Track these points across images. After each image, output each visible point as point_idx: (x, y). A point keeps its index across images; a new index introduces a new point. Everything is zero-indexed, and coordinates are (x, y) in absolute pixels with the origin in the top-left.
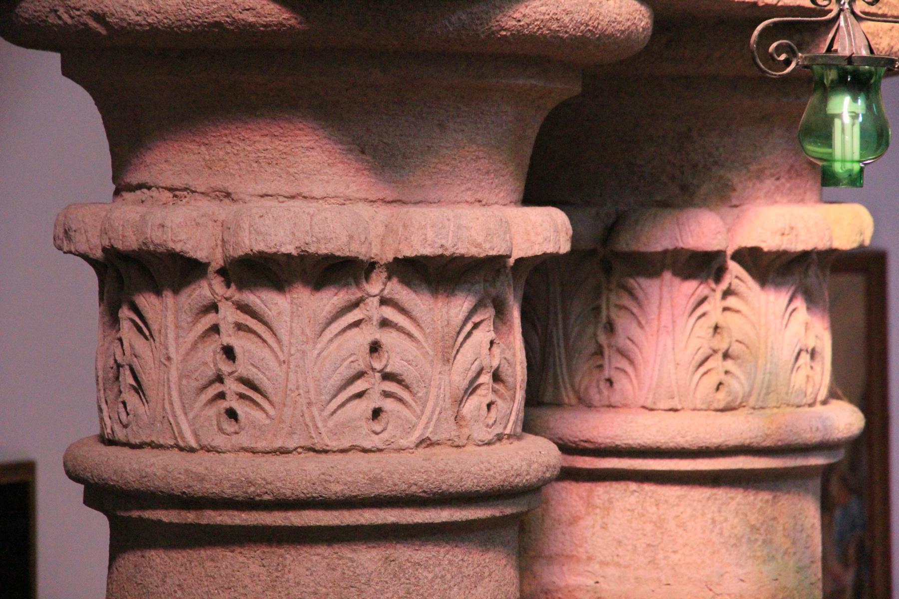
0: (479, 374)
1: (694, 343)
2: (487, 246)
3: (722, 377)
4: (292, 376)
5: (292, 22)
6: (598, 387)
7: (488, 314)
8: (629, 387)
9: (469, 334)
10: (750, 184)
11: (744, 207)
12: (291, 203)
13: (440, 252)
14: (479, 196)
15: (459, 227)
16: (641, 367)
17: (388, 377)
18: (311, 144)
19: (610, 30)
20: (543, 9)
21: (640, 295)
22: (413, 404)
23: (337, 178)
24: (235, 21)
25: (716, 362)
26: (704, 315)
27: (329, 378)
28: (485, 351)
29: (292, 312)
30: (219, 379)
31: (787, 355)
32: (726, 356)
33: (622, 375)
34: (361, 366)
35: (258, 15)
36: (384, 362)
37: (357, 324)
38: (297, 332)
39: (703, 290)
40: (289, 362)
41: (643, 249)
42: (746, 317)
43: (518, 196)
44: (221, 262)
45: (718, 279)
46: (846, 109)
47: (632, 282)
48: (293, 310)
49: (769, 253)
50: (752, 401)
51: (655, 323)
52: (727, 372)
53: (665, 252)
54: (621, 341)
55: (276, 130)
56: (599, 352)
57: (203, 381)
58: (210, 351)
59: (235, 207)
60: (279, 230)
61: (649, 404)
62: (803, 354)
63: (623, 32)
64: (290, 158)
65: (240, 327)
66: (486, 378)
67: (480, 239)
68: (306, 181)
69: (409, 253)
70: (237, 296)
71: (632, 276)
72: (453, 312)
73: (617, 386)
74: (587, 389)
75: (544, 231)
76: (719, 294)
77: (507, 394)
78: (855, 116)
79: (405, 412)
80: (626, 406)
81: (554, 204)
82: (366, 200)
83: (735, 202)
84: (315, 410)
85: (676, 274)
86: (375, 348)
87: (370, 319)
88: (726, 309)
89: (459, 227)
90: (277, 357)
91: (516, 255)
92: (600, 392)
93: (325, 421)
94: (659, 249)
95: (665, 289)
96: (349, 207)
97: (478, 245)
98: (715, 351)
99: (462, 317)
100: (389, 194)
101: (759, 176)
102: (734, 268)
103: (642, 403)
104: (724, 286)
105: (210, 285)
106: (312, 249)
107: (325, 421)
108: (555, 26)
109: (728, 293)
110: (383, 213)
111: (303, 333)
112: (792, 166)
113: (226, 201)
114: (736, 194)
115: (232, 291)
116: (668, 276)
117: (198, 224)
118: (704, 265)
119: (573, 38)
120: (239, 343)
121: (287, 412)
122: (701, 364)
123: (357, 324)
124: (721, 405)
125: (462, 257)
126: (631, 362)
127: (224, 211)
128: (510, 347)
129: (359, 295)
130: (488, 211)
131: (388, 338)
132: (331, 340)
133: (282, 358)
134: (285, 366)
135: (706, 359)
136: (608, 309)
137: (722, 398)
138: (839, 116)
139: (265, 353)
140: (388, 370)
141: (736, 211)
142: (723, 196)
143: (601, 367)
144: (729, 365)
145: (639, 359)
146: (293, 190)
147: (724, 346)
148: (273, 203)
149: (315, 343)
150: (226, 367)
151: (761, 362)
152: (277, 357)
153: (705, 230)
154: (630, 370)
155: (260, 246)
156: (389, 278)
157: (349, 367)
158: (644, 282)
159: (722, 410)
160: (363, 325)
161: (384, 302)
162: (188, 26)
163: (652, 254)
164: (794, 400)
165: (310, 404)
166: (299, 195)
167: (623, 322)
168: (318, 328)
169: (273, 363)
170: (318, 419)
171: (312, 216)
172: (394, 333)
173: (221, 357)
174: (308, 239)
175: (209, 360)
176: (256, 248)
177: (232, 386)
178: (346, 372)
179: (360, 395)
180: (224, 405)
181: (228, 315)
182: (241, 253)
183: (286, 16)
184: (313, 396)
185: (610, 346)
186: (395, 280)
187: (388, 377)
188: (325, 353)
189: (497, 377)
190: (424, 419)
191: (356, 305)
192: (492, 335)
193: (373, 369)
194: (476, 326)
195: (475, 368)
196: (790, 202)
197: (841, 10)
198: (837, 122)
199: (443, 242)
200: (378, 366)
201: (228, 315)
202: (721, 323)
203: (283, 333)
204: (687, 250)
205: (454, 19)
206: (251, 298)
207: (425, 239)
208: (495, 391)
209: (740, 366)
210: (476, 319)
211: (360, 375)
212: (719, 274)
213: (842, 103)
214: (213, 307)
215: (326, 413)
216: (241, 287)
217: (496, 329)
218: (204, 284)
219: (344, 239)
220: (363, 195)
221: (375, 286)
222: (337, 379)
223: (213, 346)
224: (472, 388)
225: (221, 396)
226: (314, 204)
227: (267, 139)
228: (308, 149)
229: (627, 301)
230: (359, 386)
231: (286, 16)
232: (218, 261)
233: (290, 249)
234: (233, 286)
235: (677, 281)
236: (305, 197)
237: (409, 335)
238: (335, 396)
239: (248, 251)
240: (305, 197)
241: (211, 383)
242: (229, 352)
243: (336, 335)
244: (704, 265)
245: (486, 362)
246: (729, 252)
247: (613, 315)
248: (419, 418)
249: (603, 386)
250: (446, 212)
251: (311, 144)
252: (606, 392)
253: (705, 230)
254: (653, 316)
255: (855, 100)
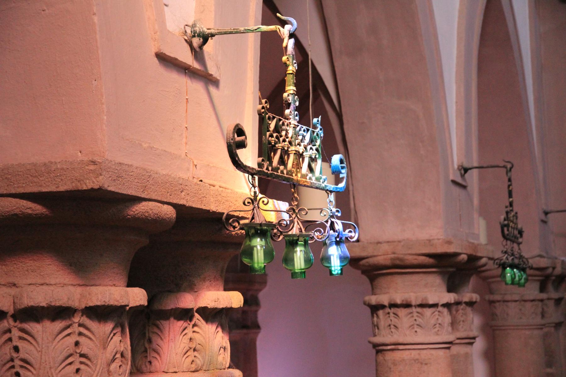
0: (116, 354)
1: (183, 345)
2: (121, 301)
3: (193, 358)
4: (43, 357)
5: (47, 213)
6: (145, 365)
7: (119, 329)
8: (157, 364)
9: (112, 338)
10: (201, 283)
11: (199, 292)
12: (41, 287)
13: (103, 304)
14: (114, 283)
15: (110, 294)
16: (163, 356)
17: (82, 355)
18: (50, 263)
19: (165, 217)
20: (143, 208)
21: (162, 328)
22: (91, 365)
23: (60, 276)
24: (23, 213)
25: (191, 353)
26: (186, 334)
27: (59, 357)
28: (118, 345)
29: (43, 331)
30: (12, 360)
31: (216, 348)
32: (195, 350)
33: (155, 359)
34: (71, 351)
35: (33, 210)
36: (80, 349)
37: (69, 335)
38: (45, 339)
39: (185, 324)
40: (42, 351)
41: (164, 309)
42: (201, 335)
43: (126, 284)
44: (13, 312)
45: (191, 320)
46: (258, 243)
47: (158, 322)
48: (42, 330)
49: (211, 309)
50: (204, 368)
51: (167, 338)
52: (195, 356)
53: (172, 309)
54: (154, 346)
55: (35, 258)
56: (146, 351)
57: (5, 361)
58: (8, 350)
59: (18, 290)
60: (39, 297)
61: (166, 370)
62: (222, 349)
63: (168, 218)
64: (41, 269)
65: (20, 338)
66: (118, 356)
67: (118, 299)
68: (48, 278)
69: (91, 304)
70: (20, 326)
71: (159, 320)
72: (106, 329)
73: (153, 364)
74: (140, 366)
75: (137, 297)
76: (191, 326)
77: (125, 362)
78: (262, 246)
79: (89, 369)
80: (157, 372)
81: (140, 287)
82: (72, 285)
83: (196, 290)
84: (53, 370)
85: (175, 318)
86: (77, 344)
87: (75, 332)
88: (194, 332)
89: (110, 294)
90: (37, 349)
91: (131, 305)
92: (146, 367)
93: (57, 374)
94: (170, 308)
95: (171, 325)
96: (65, 288)
97: (118, 301)
98: (190, 348)
99: (110, 331)
100: (81, 282)
101: (204, 280)
102: (197, 315)
103: (163, 370)
104: (193, 323)
105: (8, 322)
106: (53, 304)
107: (57, 374)
108: (147, 215)
109: (194, 325)
110: (79, 290)
111: (48, 339)
112: (215, 276)
113: (14, 287)
114: (196, 287)
115: (18, 324)
116: (172, 319)
117: (3, 297)
118: (186, 315)
119: (153, 220)
120: (21, 345)
121: (41, 371)
122: (185, 354)
123: (69, 335)
124: (193, 370)
125: (112, 306)
126: (158, 354)
127: (13, 291)
128: (126, 343)
129: (70, 323)
130: (117, 288)
131: (82, 340)
132: (59, 342)
133: (39, 349)
134: (40, 353)
135: (187, 351)
136: (149, 333)
137: (193, 367)
138: (256, 246)
139: (32, 348)
140: (82, 353)
141: (197, 293)
142: (192, 288)
143: (146, 357)
144: (196, 353)
145: (161, 353)
146: (42, 282)
147: (194, 346)
148: (34, 287)
149: (52, 343)
150: (15, 355)
151: (207, 353)
152: (37, 349)
153: (188, 301)
154: (158, 357)
155: (31, 304)
156: (82, 316)
157: (66, 352)
158: (163, 322)
159: (193, 372)
160: (71, 335)
161: (80, 325)
162: (3, 216)
163: (168, 310)
164: (219, 367)
165: (50, 368)
166: (45, 283)
167: (155, 338)
168: (54, 337)
169: (35, 352)
170: (54, 374)
171: (53, 291)
172: (84, 338)
173: (12, 351)
174: (51, 300)
175: (8, 352)
176: (30, 304)
177: (17, 363)
178: (65, 354)
179: (70, 364)
180: (15, 370)
181: (16, 333)
182: (23, 307)
183: (44, 210)
184: (52, 364)
185: (150, 348)
186: (85, 316)
187: (82, 355)
188: (57, 347)
189: (122, 355)
190: (96, 372)
191: (68, 327)
192: (120, 338)
193: (76, 352)
194: (114, 334)
195: (115, 351)
196: (215, 290)
197: (255, 207)
198: (255, 249)
199: (105, 300)
200: (78, 351)
201: (16, 333)
202: (193, 337)
203: (39, 340)
204: (181, 308)
205: (111, 211)
206: (26, 326)
207: (98, 299)
208: (122, 361)
209: (200, 354)
210: (114, 332)
211: (71, 355)
212: (191, 318)
213: (458, 160)
214: (9, 331)
215: (57, 371)
216: (21, 322)
217: (121, 336)
218: (5, 321)
219: (66, 299)
220: (71, 283)
221: (77, 319)
222: (61, 357)
223: (9, 346)
224: (113, 360)
225: (13, 367)
226: (52, 288)
227: (31, 262)
228: (49, 265)
229: (156, 330)
230: (70, 360)
231: (44, 210)
232: (11, 311)
233: (44, 304)
234: (18, 322)
235: (175, 321)
236: (47, 284)
237: (90, 338)
238: (61, 364)
239: (26, 306)
240: (47, 284)
241: (8, 362)
242: (16, 349)
243: (61, 340)
244: (186, 315)
245: (118, 349)
246: (195, 309)
247: (151, 335)
248: (94, 372)
249: (147, 364)
250: (100, 289)
251: (50, 263)
252: (148, 367)
253: (188, 301)
254: (167, 335)
255: (261, 240)
